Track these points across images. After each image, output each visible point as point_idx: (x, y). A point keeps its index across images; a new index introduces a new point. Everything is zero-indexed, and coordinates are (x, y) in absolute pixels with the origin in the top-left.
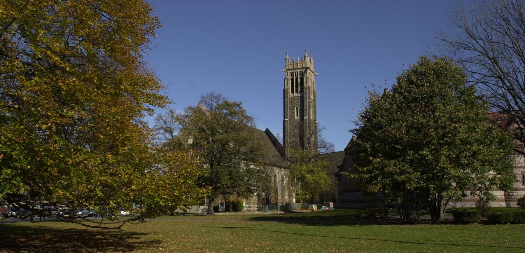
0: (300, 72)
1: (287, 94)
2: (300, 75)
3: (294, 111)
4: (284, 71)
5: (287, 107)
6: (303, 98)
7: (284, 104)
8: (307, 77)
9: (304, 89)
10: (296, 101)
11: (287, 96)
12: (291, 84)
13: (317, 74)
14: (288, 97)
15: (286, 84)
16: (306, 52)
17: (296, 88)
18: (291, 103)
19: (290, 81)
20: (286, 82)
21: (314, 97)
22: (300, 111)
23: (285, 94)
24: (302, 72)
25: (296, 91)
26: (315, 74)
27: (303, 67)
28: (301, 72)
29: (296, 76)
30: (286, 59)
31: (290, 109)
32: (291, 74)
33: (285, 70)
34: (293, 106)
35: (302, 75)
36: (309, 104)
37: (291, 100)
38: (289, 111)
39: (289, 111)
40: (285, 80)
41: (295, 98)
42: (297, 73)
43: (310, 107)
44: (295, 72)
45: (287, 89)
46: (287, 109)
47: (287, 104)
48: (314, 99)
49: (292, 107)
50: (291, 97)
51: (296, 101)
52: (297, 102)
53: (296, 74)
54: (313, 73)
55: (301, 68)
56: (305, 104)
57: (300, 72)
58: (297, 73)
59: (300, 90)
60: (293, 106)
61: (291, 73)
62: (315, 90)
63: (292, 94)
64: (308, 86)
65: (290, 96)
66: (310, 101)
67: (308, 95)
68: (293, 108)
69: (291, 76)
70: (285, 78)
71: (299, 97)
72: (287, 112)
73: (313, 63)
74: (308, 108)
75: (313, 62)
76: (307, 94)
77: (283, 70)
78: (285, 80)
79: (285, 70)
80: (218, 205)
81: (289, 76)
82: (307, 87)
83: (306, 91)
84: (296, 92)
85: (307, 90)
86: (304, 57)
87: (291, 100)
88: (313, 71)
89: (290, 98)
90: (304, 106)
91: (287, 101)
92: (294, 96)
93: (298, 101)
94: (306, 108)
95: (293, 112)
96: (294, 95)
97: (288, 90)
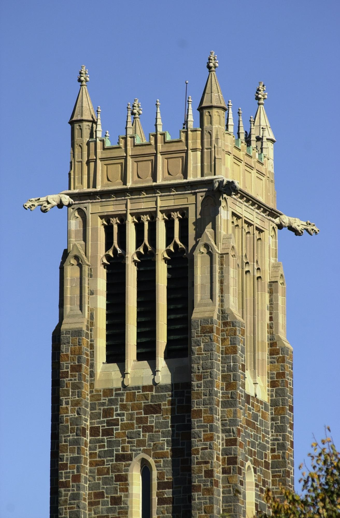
0: (168, 212)
1: (77, 368)
2: (169, 238)
3: (126, 490)
4: (60, 205)
5: (76, 460)
6: (189, 400)
7: (55, 437)
8: (218, 250)
9: (195, 333)
10: (140, 420)
11: (77, 387)
12: (109, 296)
13: (298, 224)
14: (86, 390)
15: (68, 294)
16: (85, 89)
17: (139, 325)
18: (107, 433)
19: (102, 273)
20: (68, 286)
21: (273, 384)
22: (168, 493)
23: (66, 365)
24: (184, 212)
25: (139, 345)
26: (286, 219)
27: (191, 178)
28: (176, 216)
29: (139, 241)
30: (72, 123)
31: (98, 480)
32: (109, 230)
33: (67, 200)
34: (120, 458)
35: (184, 237)
36: (231, 442)
37: (107, 413)
38: (85, 493)
39: (85, 493)
40: (62, 269)
41: (132, 397)
42: (146, 219)
43: (232, 461)
44: (138, 215)
45: (78, 333)
46: (77, 478)
47: (76, 442)
48: (274, 403)
49: (109, 463)
50: (108, 392)
51: (140, 420)
52: (147, 429)
53: (139, 227)
54: (273, 214)
55: (178, 187)
56: (197, 444)
57: (168, 212)
58: (146, 219)
59: (169, 342)
60: (120, 458)
61: (107, 218)
62: (282, 334)
63: (114, 367)
64: (223, 314)
65: (99, 386)
66: (234, 422)
67: (219, 382)
68: (115, 468)
69: (109, 244)
70: (66, 254)
71: (163, 388)
72: (76, 497)
73: (269, 149)
74: (218, 474)
75: (269, 134)
76: (218, 372)
77: (54, 199)
78: (62, 269)
79: (67, 200)
80: (337, 499)
81: (95, 239)
82: (217, 324)
83: (208, 348)
84: (140, 357)
85: (218, 345)
86: (201, 109)
87: (107, 413)
88: (272, 205)
89: (95, 397)
90: (196, 458)
91: (75, 421)
92: (129, 382)
93: (153, 419)
94: (209, 473)
95: (116, 501)
96: (123, 373)
97: (85, 340)
